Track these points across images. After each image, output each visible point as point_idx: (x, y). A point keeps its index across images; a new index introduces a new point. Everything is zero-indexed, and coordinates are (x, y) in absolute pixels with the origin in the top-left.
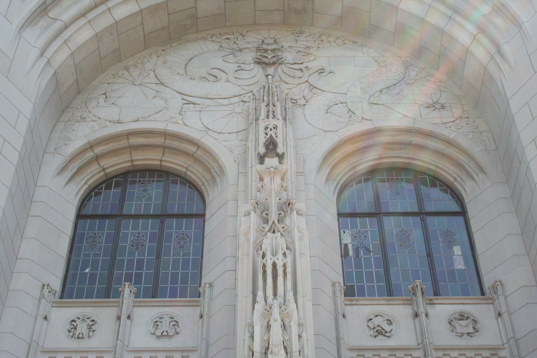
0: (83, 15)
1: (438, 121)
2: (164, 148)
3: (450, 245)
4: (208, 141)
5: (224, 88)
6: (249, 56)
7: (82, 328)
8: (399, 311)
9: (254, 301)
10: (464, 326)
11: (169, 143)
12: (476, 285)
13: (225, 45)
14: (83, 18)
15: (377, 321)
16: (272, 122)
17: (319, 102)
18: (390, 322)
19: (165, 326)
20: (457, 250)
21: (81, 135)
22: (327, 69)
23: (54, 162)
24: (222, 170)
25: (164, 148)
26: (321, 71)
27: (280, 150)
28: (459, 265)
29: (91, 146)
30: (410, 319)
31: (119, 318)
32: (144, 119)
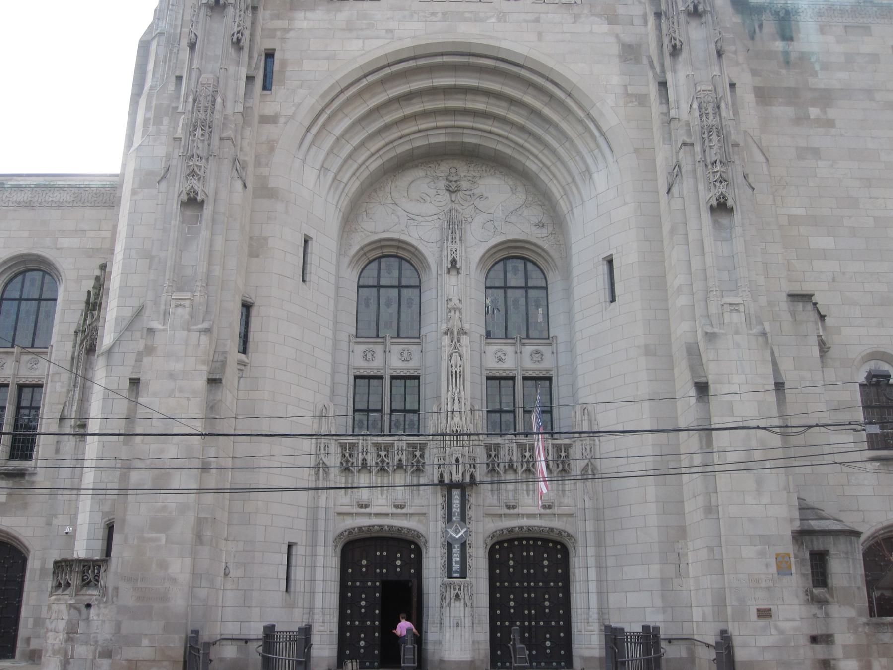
0: (354, 174)
1: (539, 236)
2: (398, 247)
3: (537, 307)
4: (421, 247)
5: (429, 209)
6: (442, 184)
7: (369, 356)
8: (509, 350)
9: (448, 390)
10: (537, 357)
11: (401, 245)
12: (548, 339)
13: (429, 173)
14: (350, 162)
15: (499, 354)
16: (454, 246)
17: (479, 219)
18: (505, 355)
19: (406, 356)
20: (540, 310)
21: (358, 241)
22: (485, 195)
23: (347, 260)
24: (429, 267)
25: (398, 247)
26: (481, 197)
27: (458, 266)
28: (540, 319)
29: (362, 248)
30: (513, 354)
31: (385, 352)
32: (388, 231)
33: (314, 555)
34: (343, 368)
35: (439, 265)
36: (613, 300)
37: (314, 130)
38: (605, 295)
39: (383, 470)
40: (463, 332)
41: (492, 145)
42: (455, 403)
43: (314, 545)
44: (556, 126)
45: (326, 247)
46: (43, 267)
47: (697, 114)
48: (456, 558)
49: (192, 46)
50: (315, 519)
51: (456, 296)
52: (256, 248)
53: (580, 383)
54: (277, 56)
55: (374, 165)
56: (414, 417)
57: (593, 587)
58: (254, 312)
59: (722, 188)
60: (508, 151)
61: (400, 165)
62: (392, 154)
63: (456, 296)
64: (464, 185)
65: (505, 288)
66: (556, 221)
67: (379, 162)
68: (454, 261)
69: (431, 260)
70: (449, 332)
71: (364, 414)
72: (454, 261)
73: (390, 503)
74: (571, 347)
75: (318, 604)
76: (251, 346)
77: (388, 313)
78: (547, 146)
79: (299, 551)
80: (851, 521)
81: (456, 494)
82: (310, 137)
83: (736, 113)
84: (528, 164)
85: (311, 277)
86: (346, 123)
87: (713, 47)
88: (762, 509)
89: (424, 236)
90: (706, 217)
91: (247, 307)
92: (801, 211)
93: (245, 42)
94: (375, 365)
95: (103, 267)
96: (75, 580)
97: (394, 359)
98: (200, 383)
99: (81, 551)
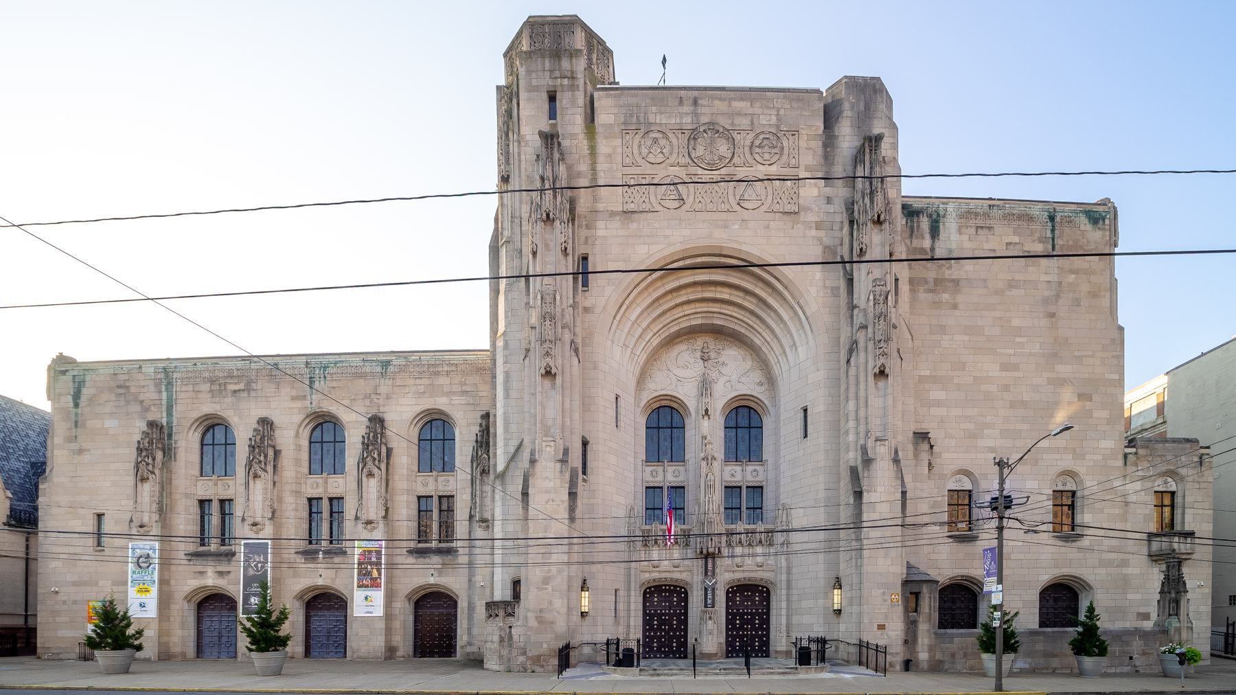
6: (699, 354)
8: (738, 469)
17: (722, 380)
21: (646, 396)
33: (629, 596)
34: (640, 483)
35: (697, 412)
36: (806, 436)
37: (618, 318)
38: (801, 433)
39: (750, 545)
40: (714, 458)
41: (732, 326)
42: (708, 504)
43: (629, 590)
44: (775, 311)
45: (627, 401)
46: (443, 417)
47: (871, 303)
48: (710, 596)
49: (534, 254)
50: (629, 575)
51: (706, 432)
52: (587, 405)
53: (782, 489)
54: (590, 259)
55: (655, 342)
56: (681, 512)
57: (784, 612)
58: (589, 447)
59: (882, 360)
60: (743, 330)
61: (671, 341)
62: (667, 333)
63: (706, 432)
64: (713, 355)
65: (737, 428)
66: (770, 380)
67: (659, 340)
68: (707, 410)
69: (692, 409)
70: (705, 459)
71: (653, 511)
72: (707, 410)
73: (670, 563)
74: (777, 467)
75: (632, 623)
76: (589, 470)
77: (665, 444)
78: (768, 327)
79: (621, 593)
80: (933, 574)
81: (710, 561)
82: (616, 322)
83: (896, 301)
84: (755, 340)
85: (621, 424)
86: (639, 310)
87: (887, 248)
88: (884, 568)
89: (687, 393)
90: (871, 379)
91: (585, 444)
92: (927, 373)
93: (570, 250)
94: (658, 480)
95: (486, 416)
96: (501, 613)
97: (669, 475)
98: (566, 497)
99: (498, 596)
